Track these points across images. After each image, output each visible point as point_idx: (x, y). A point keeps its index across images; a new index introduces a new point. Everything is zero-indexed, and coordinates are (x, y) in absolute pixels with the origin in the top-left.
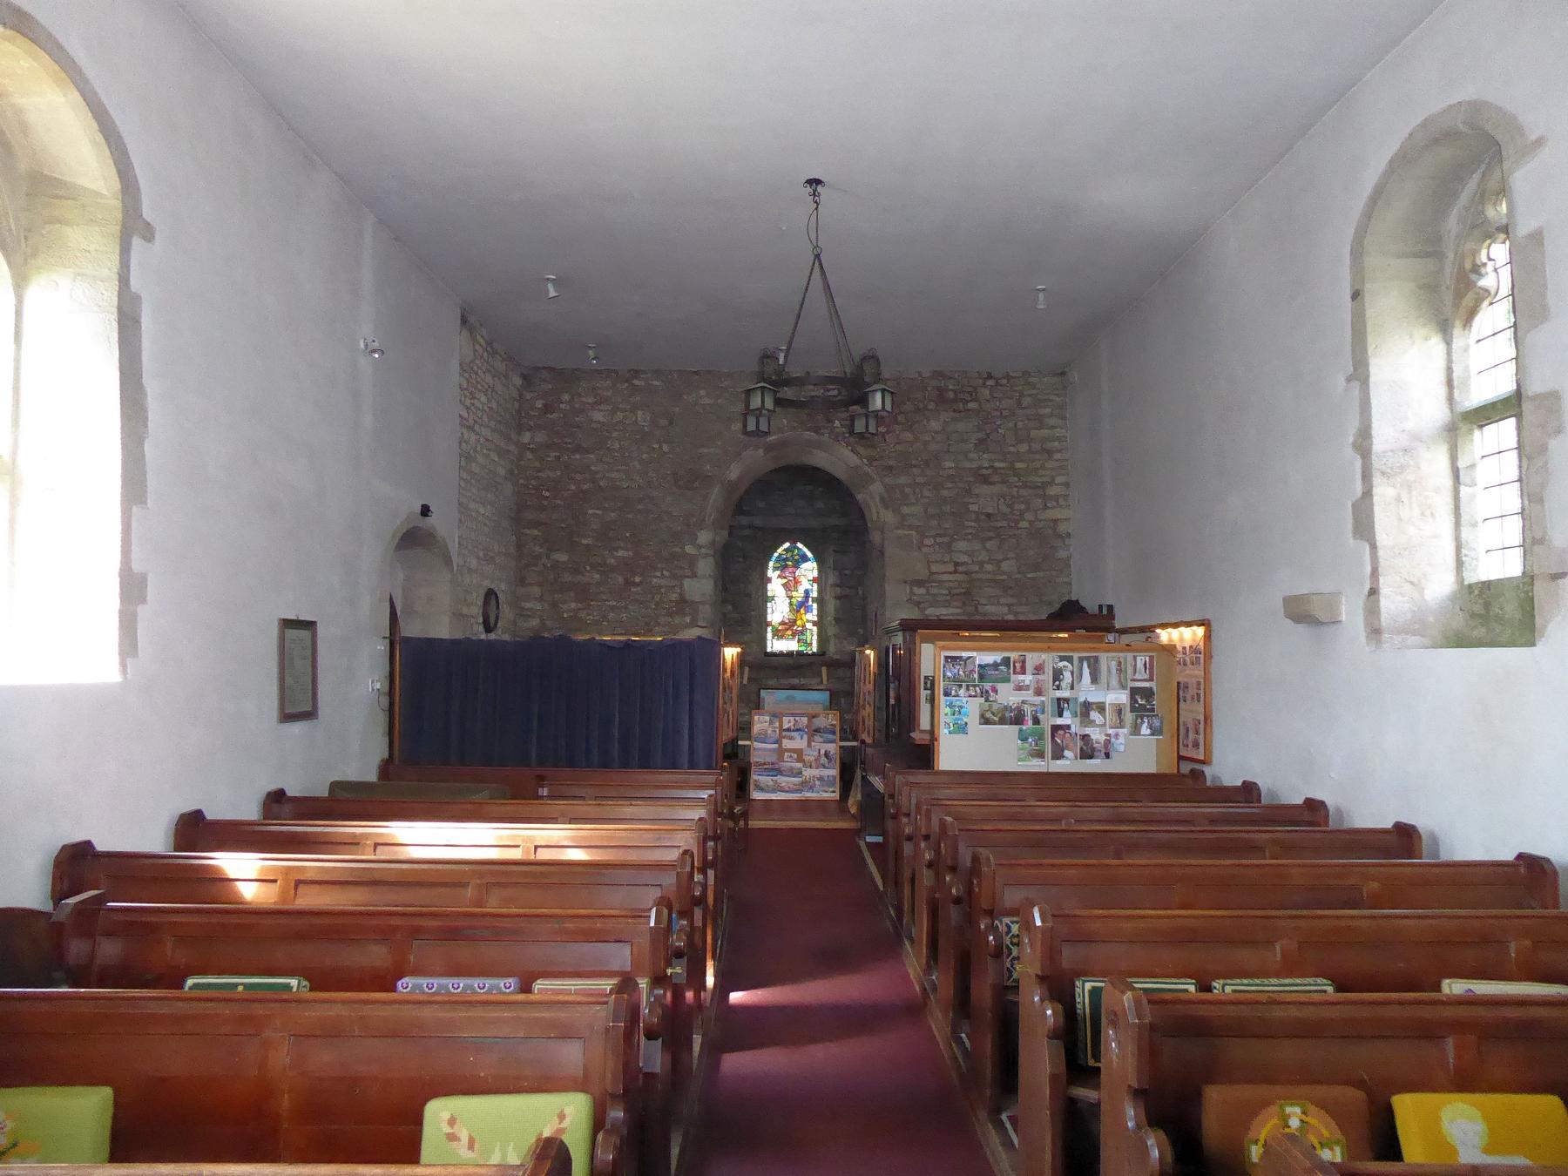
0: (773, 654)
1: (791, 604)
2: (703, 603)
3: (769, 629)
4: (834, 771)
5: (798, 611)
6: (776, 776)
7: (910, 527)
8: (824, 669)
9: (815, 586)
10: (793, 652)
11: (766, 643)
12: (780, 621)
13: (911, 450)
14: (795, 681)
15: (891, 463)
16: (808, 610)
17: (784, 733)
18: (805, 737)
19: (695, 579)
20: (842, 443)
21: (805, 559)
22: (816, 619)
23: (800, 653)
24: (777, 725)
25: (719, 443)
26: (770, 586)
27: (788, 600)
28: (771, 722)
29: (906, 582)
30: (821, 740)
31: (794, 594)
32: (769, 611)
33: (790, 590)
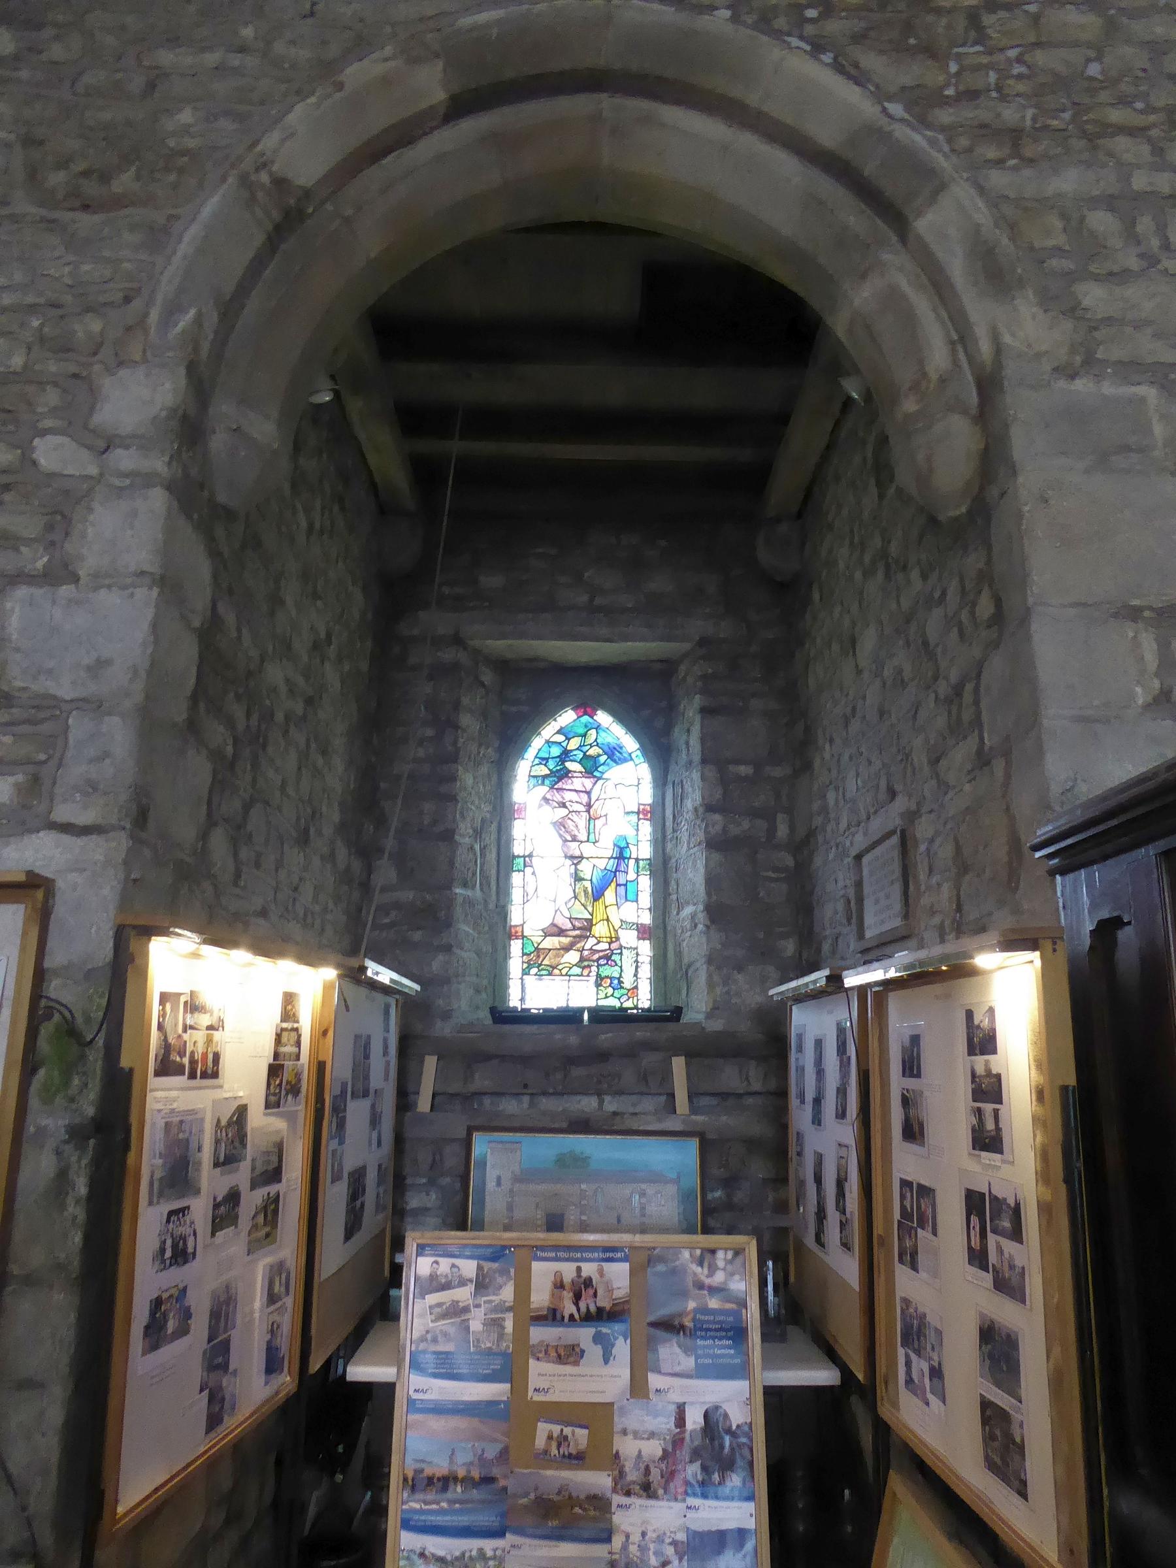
0: (524, 1018)
1: (578, 878)
2: (95, 706)
3: (516, 947)
4: (750, 1507)
5: (598, 895)
6: (499, 1533)
7: (1131, 369)
8: (678, 1064)
9: (646, 828)
10: (581, 1011)
11: (507, 987)
12: (546, 923)
13: (1094, 70)
14: (587, 1104)
15: (1010, 114)
16: (627, 894)
17: (538, 1334)
18: (622, 1349)
19: (66, 591)
20: (795, 42)
21: (614, 754)
22: (646, 919)
23: (600, 1016)
24: (507, 1293)
25: (248, 32)
26: (518, 829)
27: (568, 868)
28: (482, 1284)
29: (1134, 614)
30: (689, 1363)
31: (587, 850)
32: (516, 895)
33: (574, 839)
